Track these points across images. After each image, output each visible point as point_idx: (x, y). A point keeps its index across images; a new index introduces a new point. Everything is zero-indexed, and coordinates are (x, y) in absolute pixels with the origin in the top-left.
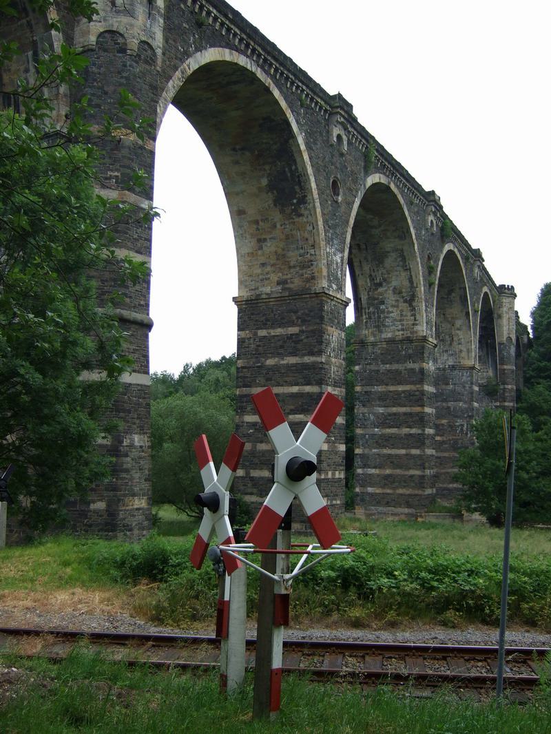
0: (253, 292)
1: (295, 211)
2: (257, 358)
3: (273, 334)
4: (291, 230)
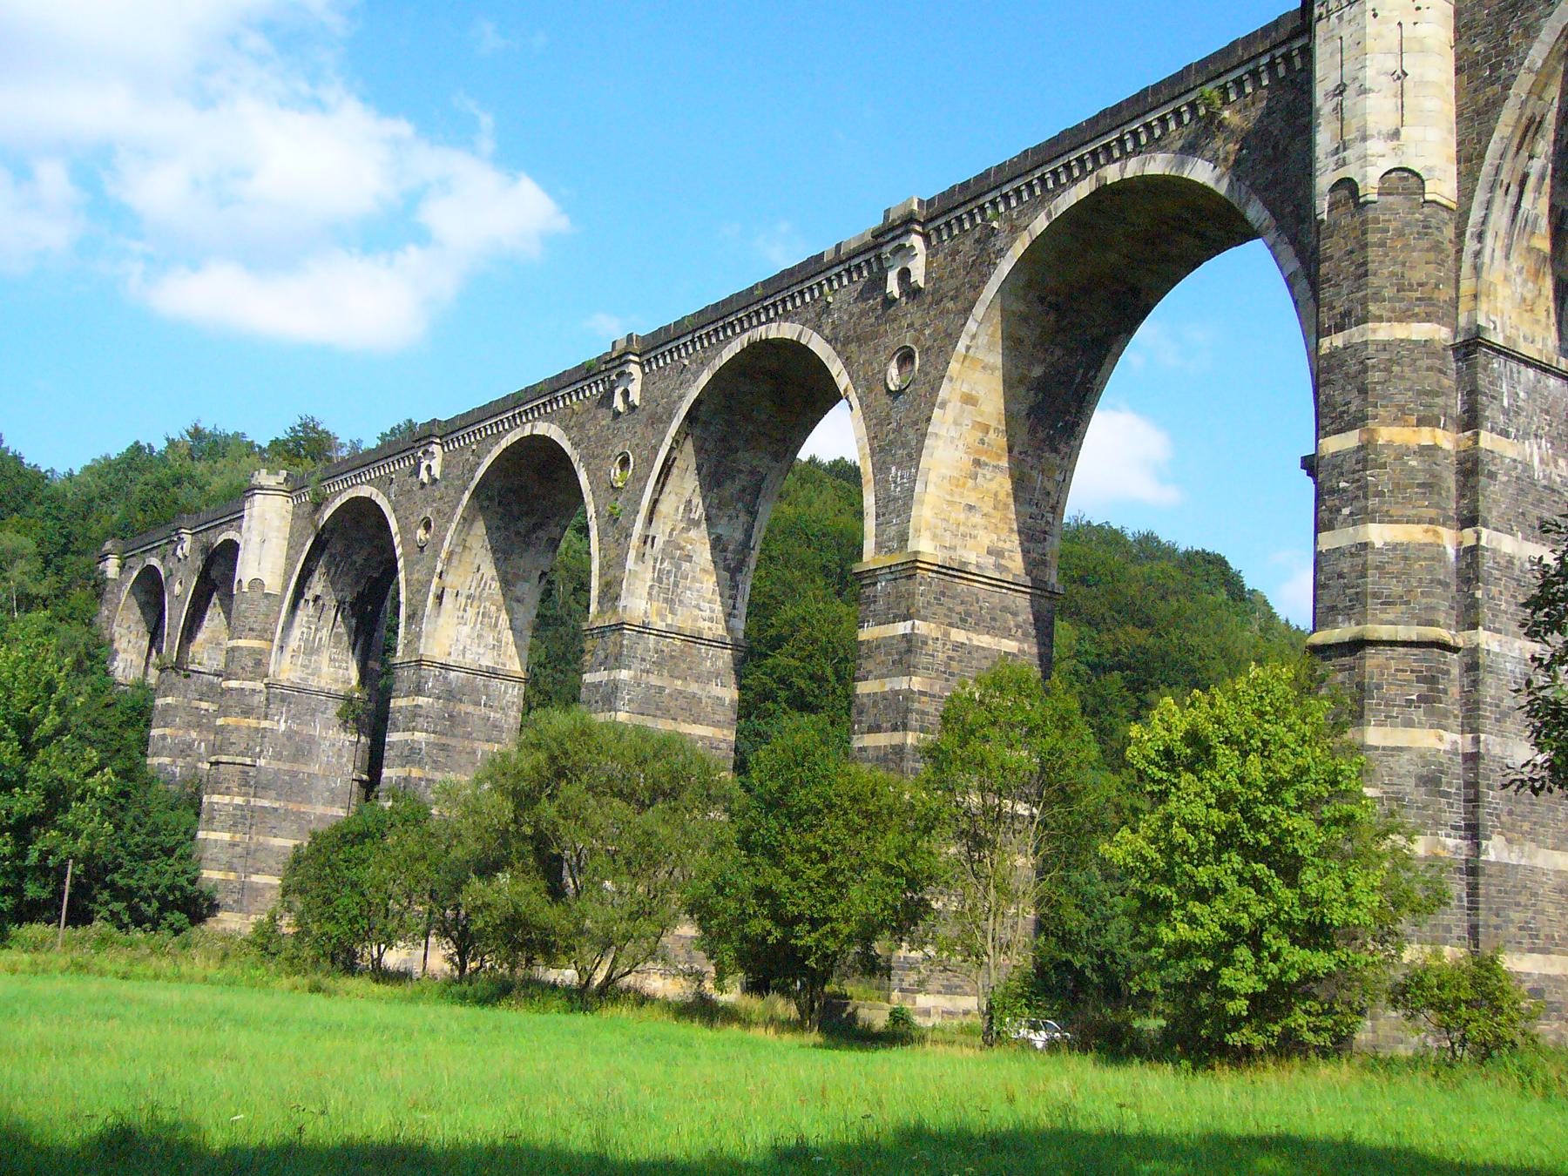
0: (946, 554)
1: (1051, 439)
2: (947, 680)
3: (975, 643)
4: (1032, 467)
